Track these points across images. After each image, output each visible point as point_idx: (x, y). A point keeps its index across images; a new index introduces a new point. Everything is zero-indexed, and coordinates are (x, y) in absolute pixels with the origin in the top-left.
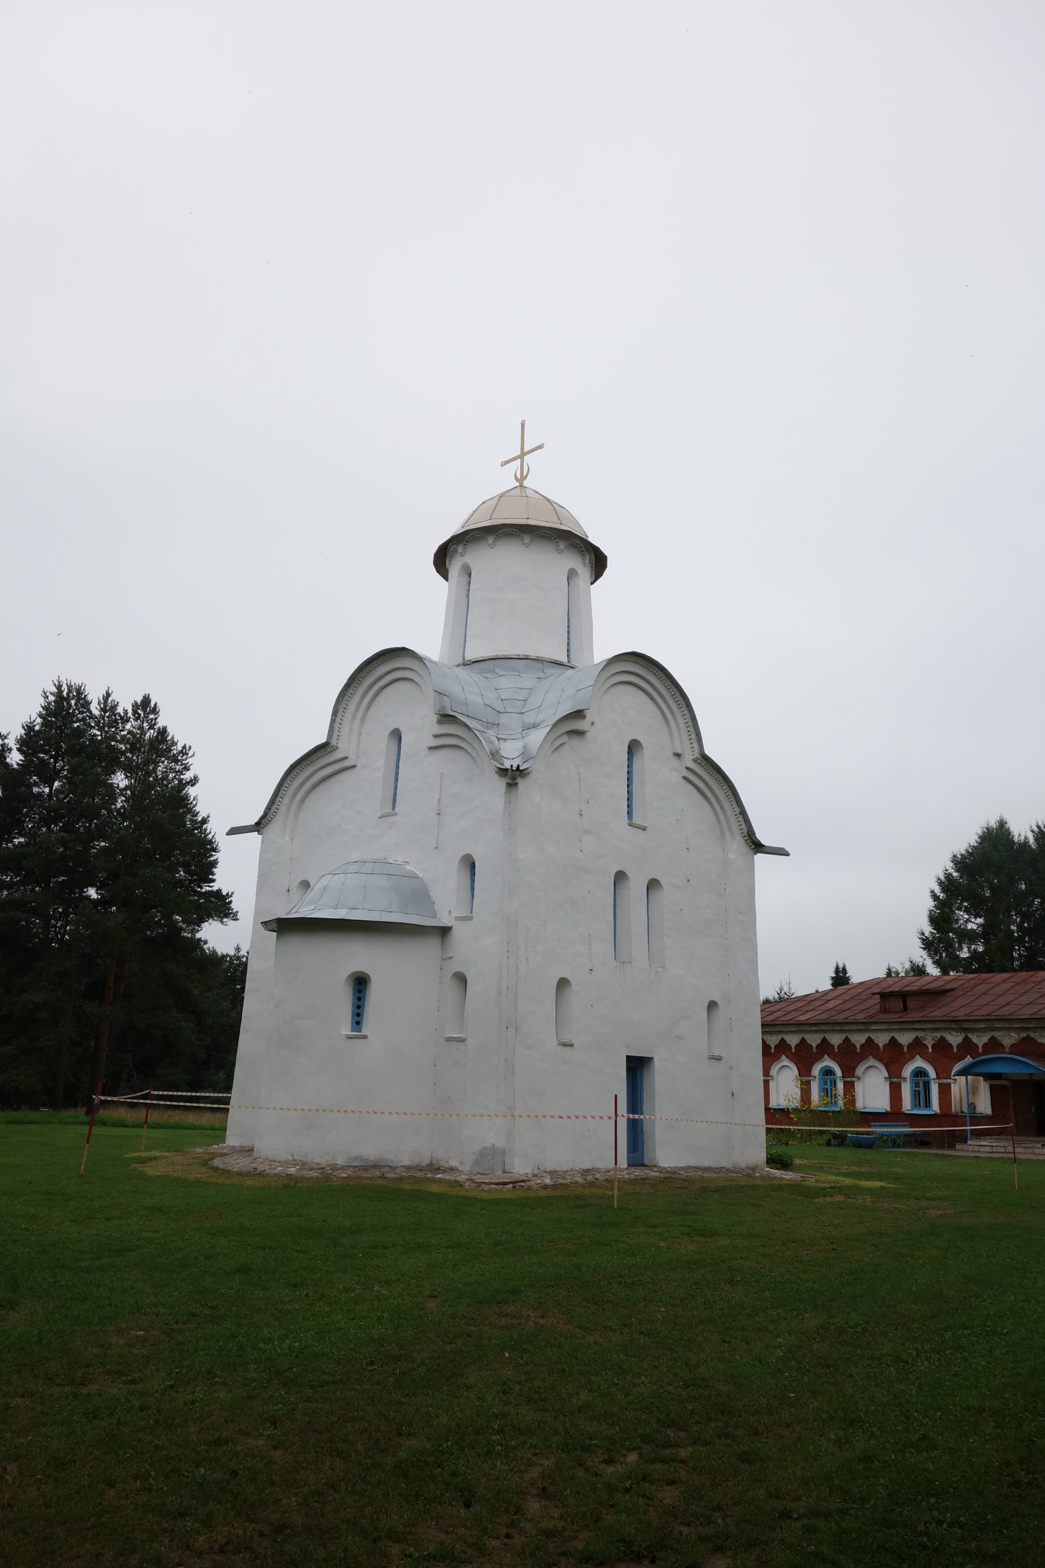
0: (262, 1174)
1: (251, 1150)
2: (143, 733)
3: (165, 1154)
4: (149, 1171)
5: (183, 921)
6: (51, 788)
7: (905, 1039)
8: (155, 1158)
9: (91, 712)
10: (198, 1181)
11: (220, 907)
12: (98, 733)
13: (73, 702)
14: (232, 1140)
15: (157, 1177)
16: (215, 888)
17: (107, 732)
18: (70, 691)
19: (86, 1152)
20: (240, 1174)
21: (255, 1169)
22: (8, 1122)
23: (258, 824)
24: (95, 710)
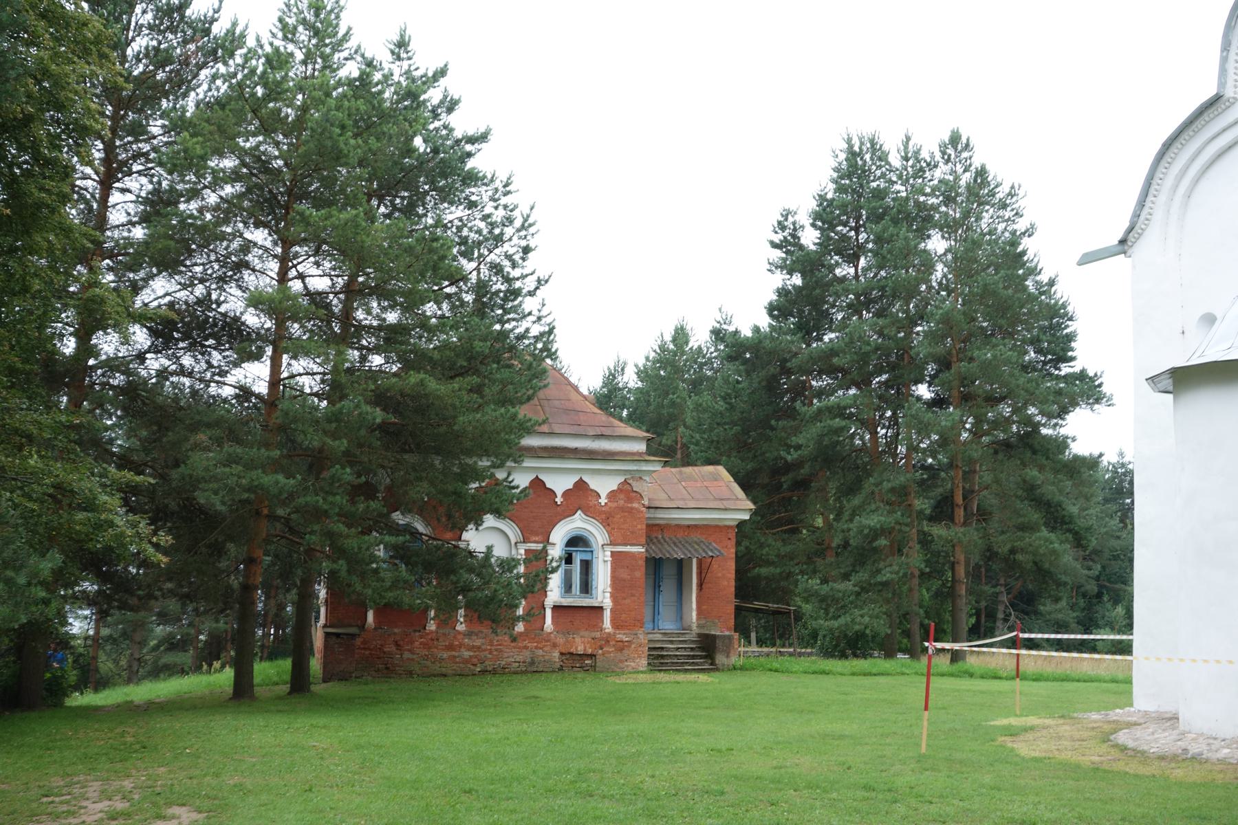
0: (1196, 759)
1: (1175, 718)
2: (957, 178)
3: (1048, 722)
4: (1024, 748)
5: (1042, 413)
6: (856, 267)
7: (560, 484)
8: (1032, 728)
9: (888, 163)
10: (1096, 769)
11: (1087, 390)
12: (903, 188)
13: (867, 157)
14: (1144, 699)
15: (1035, 760)
16: (1077, 369)
17: (913, 186)
18: (862, 143)
19: (925, 723)
20: (1162, 758)
21: (1185, 750)
22: (853, 674)
23: (1123, 242)
24: (895, 160)
